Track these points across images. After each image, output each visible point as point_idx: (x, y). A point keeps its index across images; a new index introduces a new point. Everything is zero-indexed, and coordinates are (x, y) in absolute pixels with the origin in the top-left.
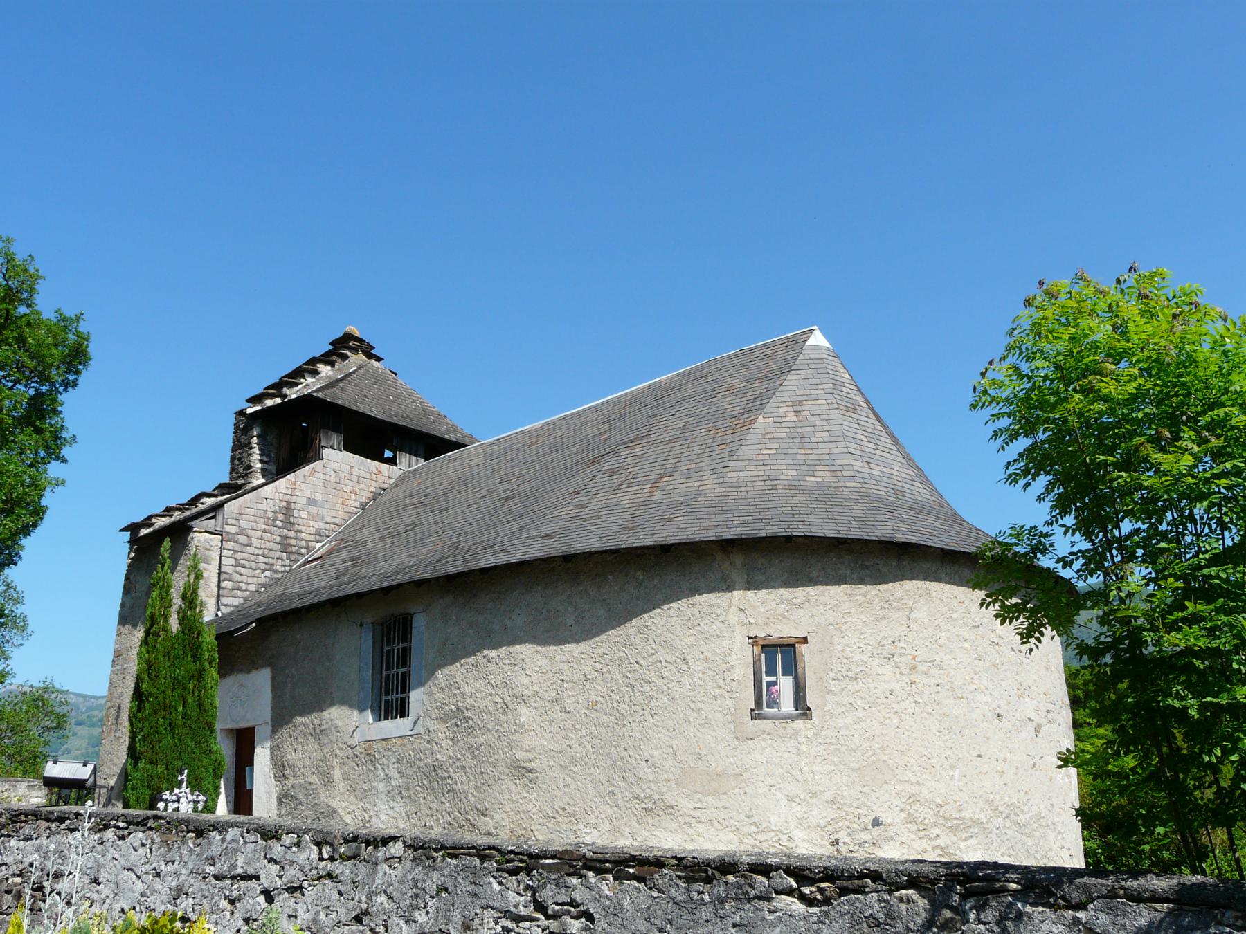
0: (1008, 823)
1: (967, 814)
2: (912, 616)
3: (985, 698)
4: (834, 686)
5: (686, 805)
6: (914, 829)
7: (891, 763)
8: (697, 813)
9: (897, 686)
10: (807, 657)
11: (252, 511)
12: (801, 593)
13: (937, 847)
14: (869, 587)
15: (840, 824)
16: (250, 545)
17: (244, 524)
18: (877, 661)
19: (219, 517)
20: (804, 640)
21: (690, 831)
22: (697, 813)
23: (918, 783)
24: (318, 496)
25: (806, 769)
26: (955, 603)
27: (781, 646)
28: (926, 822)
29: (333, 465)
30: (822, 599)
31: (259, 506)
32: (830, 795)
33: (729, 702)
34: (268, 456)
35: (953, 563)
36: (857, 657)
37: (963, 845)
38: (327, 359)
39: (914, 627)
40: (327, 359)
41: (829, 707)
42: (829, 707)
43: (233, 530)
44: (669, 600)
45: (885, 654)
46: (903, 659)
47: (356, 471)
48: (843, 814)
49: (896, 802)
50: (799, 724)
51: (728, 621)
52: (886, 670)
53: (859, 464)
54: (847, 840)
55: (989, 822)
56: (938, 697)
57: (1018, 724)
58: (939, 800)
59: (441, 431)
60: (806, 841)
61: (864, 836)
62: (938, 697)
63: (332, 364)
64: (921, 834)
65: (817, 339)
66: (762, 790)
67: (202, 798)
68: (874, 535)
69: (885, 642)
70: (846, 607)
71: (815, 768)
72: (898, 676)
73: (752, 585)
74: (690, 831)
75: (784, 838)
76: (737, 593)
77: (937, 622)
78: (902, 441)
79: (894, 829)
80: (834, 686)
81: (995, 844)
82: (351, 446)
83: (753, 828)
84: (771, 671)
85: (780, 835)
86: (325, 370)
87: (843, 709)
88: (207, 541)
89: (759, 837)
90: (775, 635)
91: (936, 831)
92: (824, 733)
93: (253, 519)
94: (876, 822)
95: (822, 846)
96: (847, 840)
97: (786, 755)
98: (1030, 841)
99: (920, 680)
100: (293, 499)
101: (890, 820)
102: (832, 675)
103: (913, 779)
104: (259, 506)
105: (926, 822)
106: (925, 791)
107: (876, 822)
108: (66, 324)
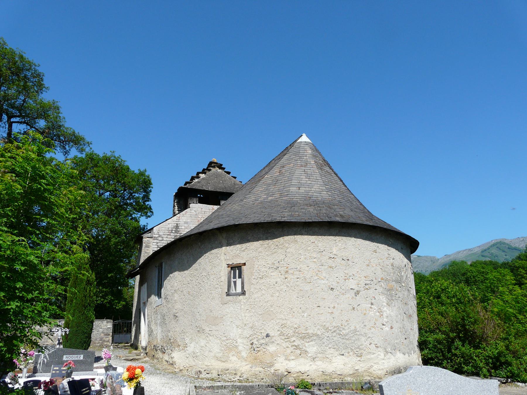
0: (335, 334)
1: (310, 331)
2: (288, 251)
3: (323, 282)
4: (254, 281)
5: (207, 329)
6: (283, 338)
7: (274, 311)
8: (210, 332)
9: (278, 280)
11: (163, 229)
12: (244, 246)
13: (293, 346)
14: (270, 241)
16: (163, 240)
17: (160, 233)
18: (271, 270)
20: (245, 264)
21: (208, 339)
22: (210, 332)
23: (286, 319)
24: (188, 221)
25: (243, 315)
26: (309, 243)
27: (237, 267)
28: (289, 335)
30: (252, 247)
32: (251, 325)
33: (220, 290)
34: (181, 208)
36: (263, 269)
37: (307, 344)
38: (204, 172)
39: (289, 255)
40: (204, 172)
43: (157, 236)
44: (206, 253)
45: (275, 267)
46: (283, 268)
47: (203, 210)
50: (241, 297)
51: (216, 261)
52: (275, 273)
53: (295, 188)
54: (256, 343)
55: (322, 334)
56: (298, 283)
57: (344, 291)
58: (296, 326)
59: (229, 191)
61: (262, 341)
62: (298, 283)
63: (205, 173)
64: (286, 340)
65: (304, 138)
66: (228, 323)
67: (67, 330)
69: (275, 262)
70: (260, 249)
71: (246, 314)
72: (280, 276)
73: (229, 244)
74: (208, 339)
75: (235, 342)
76: (224, 248)
77: (299, 252)
78: (338, 175)
80: (254, 281)
81: (326, 344)
82: (201, 201)
84: (235, 277)
86: (202, 176)
89: (227, 342)
90: (235, 263)
91: (294, 339)
94: (268, 336)
95: (247, 345)
96: (256, 343)
97: (236, 310)
98: (348, 342)
99: (290, 277)
100: (179, 223)
101: (273, 335)
102: (253, 277)
103: (284, 318)
105: (289, 335)
106: (289, 322)
107: (268, 336)
108: (142, 174)
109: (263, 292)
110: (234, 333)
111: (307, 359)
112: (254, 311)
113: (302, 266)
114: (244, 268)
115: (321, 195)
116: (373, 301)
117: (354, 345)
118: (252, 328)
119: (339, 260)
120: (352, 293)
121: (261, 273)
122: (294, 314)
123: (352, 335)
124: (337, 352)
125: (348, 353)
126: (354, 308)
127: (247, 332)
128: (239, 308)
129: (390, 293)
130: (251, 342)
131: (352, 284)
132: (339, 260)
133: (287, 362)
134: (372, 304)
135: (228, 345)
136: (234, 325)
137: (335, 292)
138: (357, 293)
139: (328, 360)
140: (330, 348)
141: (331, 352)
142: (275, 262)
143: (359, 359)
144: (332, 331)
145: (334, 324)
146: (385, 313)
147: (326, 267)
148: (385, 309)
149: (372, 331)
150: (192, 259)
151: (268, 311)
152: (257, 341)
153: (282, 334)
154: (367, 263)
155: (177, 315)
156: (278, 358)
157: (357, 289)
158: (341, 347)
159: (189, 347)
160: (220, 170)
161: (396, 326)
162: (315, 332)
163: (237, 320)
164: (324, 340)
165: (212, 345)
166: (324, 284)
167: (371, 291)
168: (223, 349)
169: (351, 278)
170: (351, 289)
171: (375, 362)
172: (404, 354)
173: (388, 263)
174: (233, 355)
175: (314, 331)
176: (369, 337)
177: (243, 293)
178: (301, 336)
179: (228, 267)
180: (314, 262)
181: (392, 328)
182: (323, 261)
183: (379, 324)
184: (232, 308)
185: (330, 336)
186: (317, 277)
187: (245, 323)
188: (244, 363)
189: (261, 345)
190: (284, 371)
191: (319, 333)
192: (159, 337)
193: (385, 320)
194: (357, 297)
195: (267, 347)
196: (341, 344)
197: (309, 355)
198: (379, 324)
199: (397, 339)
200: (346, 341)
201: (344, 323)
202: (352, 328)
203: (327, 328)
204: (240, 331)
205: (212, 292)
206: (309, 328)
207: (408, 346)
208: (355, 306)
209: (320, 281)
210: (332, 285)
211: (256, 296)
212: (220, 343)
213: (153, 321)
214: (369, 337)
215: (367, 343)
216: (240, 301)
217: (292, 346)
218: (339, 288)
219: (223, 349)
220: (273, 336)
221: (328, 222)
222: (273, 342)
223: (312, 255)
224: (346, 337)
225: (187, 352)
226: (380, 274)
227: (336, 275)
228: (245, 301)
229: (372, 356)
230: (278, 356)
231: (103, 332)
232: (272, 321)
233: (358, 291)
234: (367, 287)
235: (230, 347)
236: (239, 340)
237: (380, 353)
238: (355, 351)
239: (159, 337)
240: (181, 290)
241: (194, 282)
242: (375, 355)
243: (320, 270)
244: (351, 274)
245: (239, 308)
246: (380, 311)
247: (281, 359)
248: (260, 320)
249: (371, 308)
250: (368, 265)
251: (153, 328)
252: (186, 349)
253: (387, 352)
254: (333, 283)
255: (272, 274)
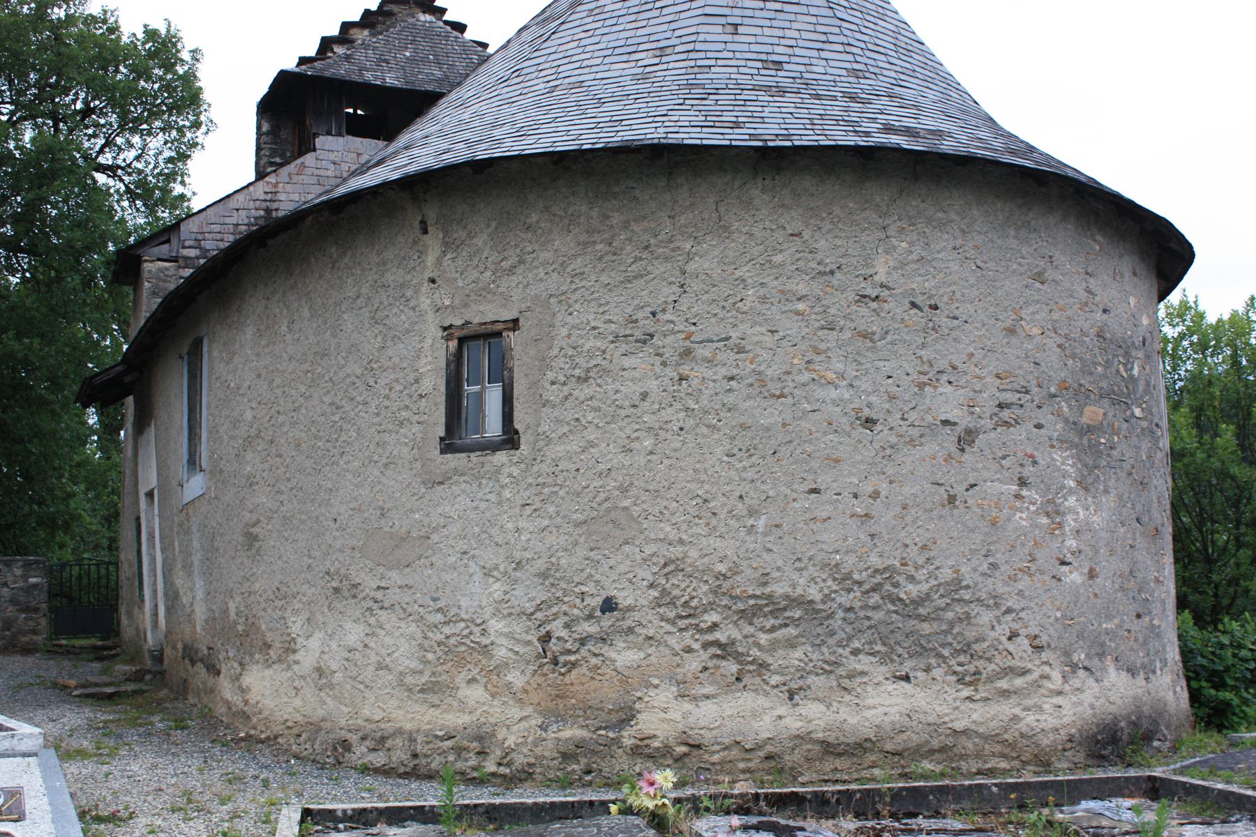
0: (875, 599)
1: (779, 589)
2: (691, 267)
3: (834, 394)
4: (552, 393)
5: (369, 583)
6: (672, 615)
7: (636, 511)
8: (379, 595)
9: (653, 385)
10: (518, 351)
11: (217, 228)
15: (555, 609)
18: (623, 348)
19: (174, 241)
20: (514, 324)
21: (372, 620)
22: (379, 595)
23: (681, 541)
28: (694, 603)
29: (332, 156)
31: (228, 220)
32: (540, 565)
33: (416, 429)
35: (779, 170)
39: (696, 286)
41: (544, 427)
42: (544, 427)
45: (638, 334)
46: (669, 340)
48: (559, 594)
49: (642, 573)
50: (501, 457)
52: (639, 361)
54: (564, 633)
55: (827, 598)
57: (915, 432)
58: (721, 568)
60: (507, 635)
62: (730, 399)
64: (682, 623)
68: (738, 138)
69: (640, 315)
70: (577, 264)
72: (658, 369)
74: (372, 620)
75: (477, 630)
77: (738, 273)
79: (637, 615)
80: (552, 393)
82: (356, 128)
83: (439, 617)
85: (473, 627)
87: (566, 429)
88: (161, 270)
89: (447, 630)
90: (476, 321)
92: (536, 468)
93: (219, 236)
94: (609, 606)
95: (529, 643)
96: (564, 633)
97: (483, 505)
98: (926, 628)
99: (696, 372)
101: (629, 601)
102: (550, 375)
103: (673, 535)
104: (228, 220)
105: (694, 603)
106: (693, 554)
107: (609, 606)
109: (591, 434)
110: (477, 595)
111: (767, 694)
112: (551, 509)
113: (750, 331)
114: (512, 338)
115: (824, 55)
116: (1028, 471)
117: (950, 639)
118: (544, 575)
119: (896, 307)
120: (948, 440)
121: (580, 360)
122: (714, 522)
123: (941, 603)
124: (883, 669)
125: (927, 670)
126: (952, 499)
127: (528, 594)
128: (492, 497)
129: (1087, 443)
130: (543, 631)
131: (948, 402)
132: (896, 307)
133: (687, 706)
134: (1023, 482)
135: (452, 641)
136: (473, 567)
137: (883, 435)
138: (967, 439)
139: (847, 698)
140: (855, 652)
141: (859, 667)
142: (640, 315)
143: (966, 692)
144: (867, 587)
145: (875, 561)
146: (1069, 518)
147: (847, 335)
148: (1071, 501)
149: (1020, 586)
150: (306, 313)
151: (608, 511)
152: (567, 626)
153: (665, 599)
154: (1009, 323)
155: (255, 530)
156: (652, 692)
157: (965, 421)
158: (900, 651)
159: (302, 653)
160: (428, 17)
161: (1109, 567)
162: (799, 591)
163: (485, 549)
164: (837, 623)
165: (388, 640)
166: (835, 403)
167: (1018, 434)
168: (430, 656)
169: (945, 378)
170: (946, 423)
171: (1029, 702)
172: (1132, 671)
173: (1086, 326)
174: (471, 681)
175: (794, 586)
176: (1009, 611)
177: (510, 439)
178: (741, 606)
179: (448, 338)
180: (798, 313)
181: (1092, 575)
182: (833, 311)
183: (1045, 558)
184: (464, 501)
185: (857, 604)
186: (806, 376)
187: (518, 555)
188: (515, 712)
189: (583, 641)
190: (672, 742)
191: (814, 593)
192: (200, 613)
193: (1072, 543)
194: (966, 456)
195: (605, 650)
196: (899, 636)
197: (775, 679)
198: (1045, 558)
199: (1109, 617)
200: (910, 622)
201: (913, 552)
202: (946, 574)
203: (848, 576)
204: (497, 589)
205: (386, 437)
206: (776, 574)
207: (1145, 643)
208: (959, 489)
209: (820, 393)
210: (869, 405)
211: (560, 449)
212: (419, 635)
213: (179, 559)
214: (1009, 611)
215: (1002, 630)
216: (498, 471)
217: (706, 646)
218: (895, 420)
219: (430, 656)
220: (630, 609)
221: (856, 149)
222: (631, 630)
223: (791, 286)
224: (921, 611)
225: (296, 668)
226: (1055, 366)
227: (886, 367)
228: (515, 471)
229: (1019, 682)
230: (649, 685)
231: (13, 601)
232: (627, 548)
233: (969, 432)
234: (1005, 414)
235: (462, 651)
236: (495, 625)
237: (1047, 669)
238: (953, 662)
239: (200, 613)
240: (267, 435)
241: (315, 402)
242: (1029, 678)
243: (823, 346)
244: (943, 364)
245: (492, 497)
246: (1053, 511)
247: (663, 696)
248: (576, 544)
249: (1018, 496)
250: (1011, 331)
251: (179, 582)
252: (292, 657)
253: (1074, 667)
254: (873, 399)
255: (627, 362)
